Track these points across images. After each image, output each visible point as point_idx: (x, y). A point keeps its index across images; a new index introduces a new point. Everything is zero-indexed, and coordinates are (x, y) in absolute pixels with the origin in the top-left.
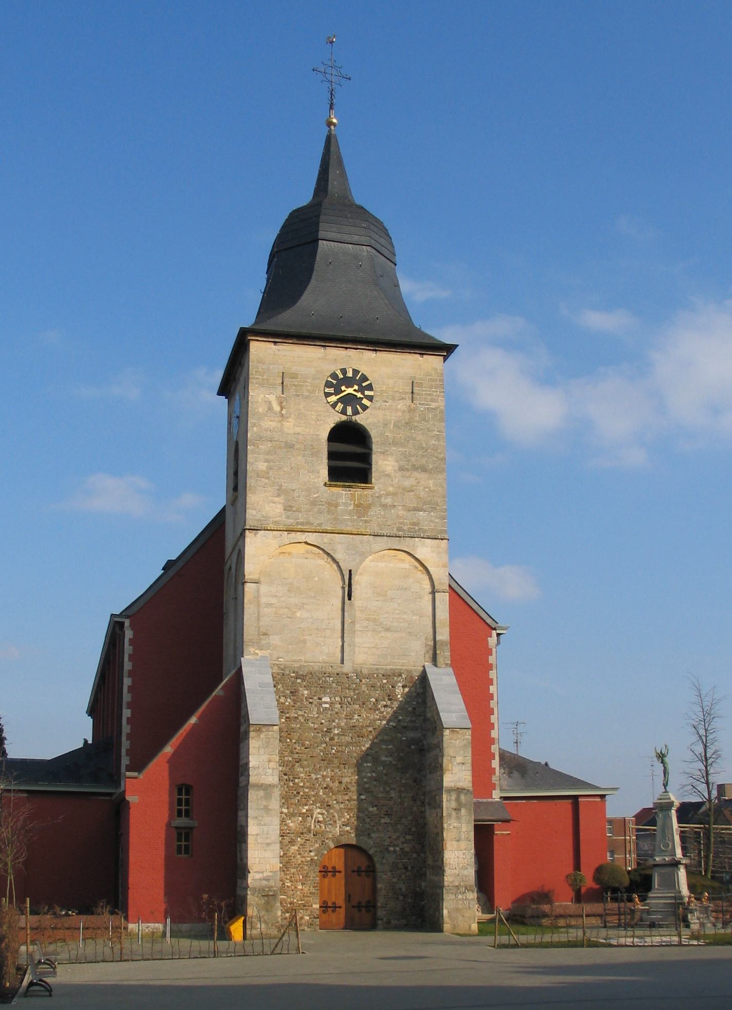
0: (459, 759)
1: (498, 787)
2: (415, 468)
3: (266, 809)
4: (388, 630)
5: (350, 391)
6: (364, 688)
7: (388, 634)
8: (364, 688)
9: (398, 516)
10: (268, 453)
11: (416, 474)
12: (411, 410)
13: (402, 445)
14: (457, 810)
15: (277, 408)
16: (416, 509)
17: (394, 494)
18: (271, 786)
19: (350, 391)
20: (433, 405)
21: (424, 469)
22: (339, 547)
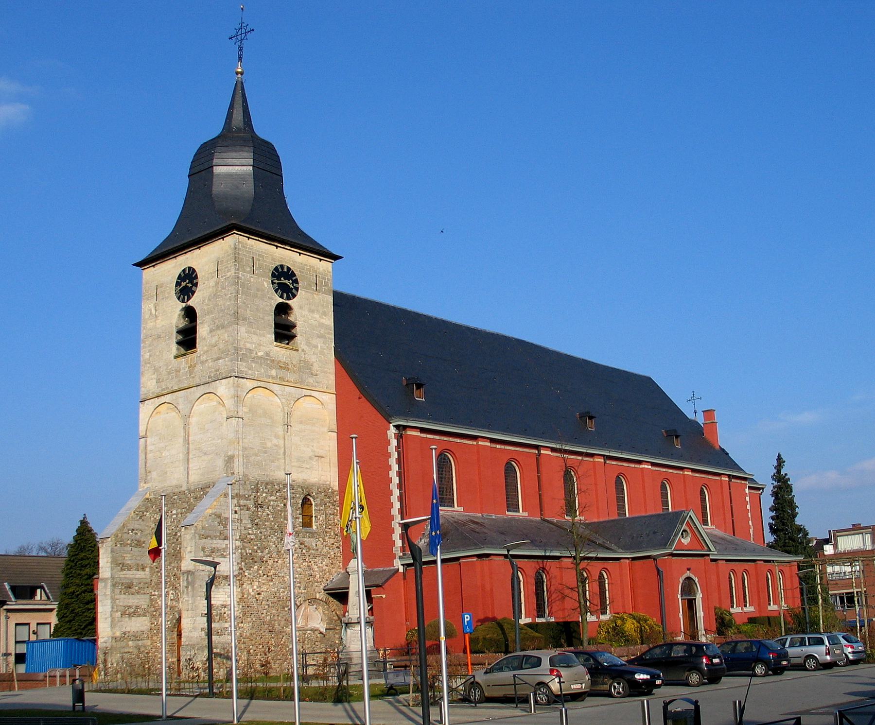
0: (189, 549)
1: (397, 557)
2: (218, 328)
3: (105, 595)
4: (205, 454)
5: (287, 282)
6: (192, 500)
7: (205, 458)
8: (192, 500)
9: (209, 368)
10: (150, 346)
11: (219, 332)
12: (217, 284)
13: (212, 313)
14: (187, 587)
15: (153, 312)
16: (218, 359)
17: (207, 352)
18: (107, 579)
19: (287, 282)
20: (229, 274)
21: (223, 327)
22: (180, 400)
